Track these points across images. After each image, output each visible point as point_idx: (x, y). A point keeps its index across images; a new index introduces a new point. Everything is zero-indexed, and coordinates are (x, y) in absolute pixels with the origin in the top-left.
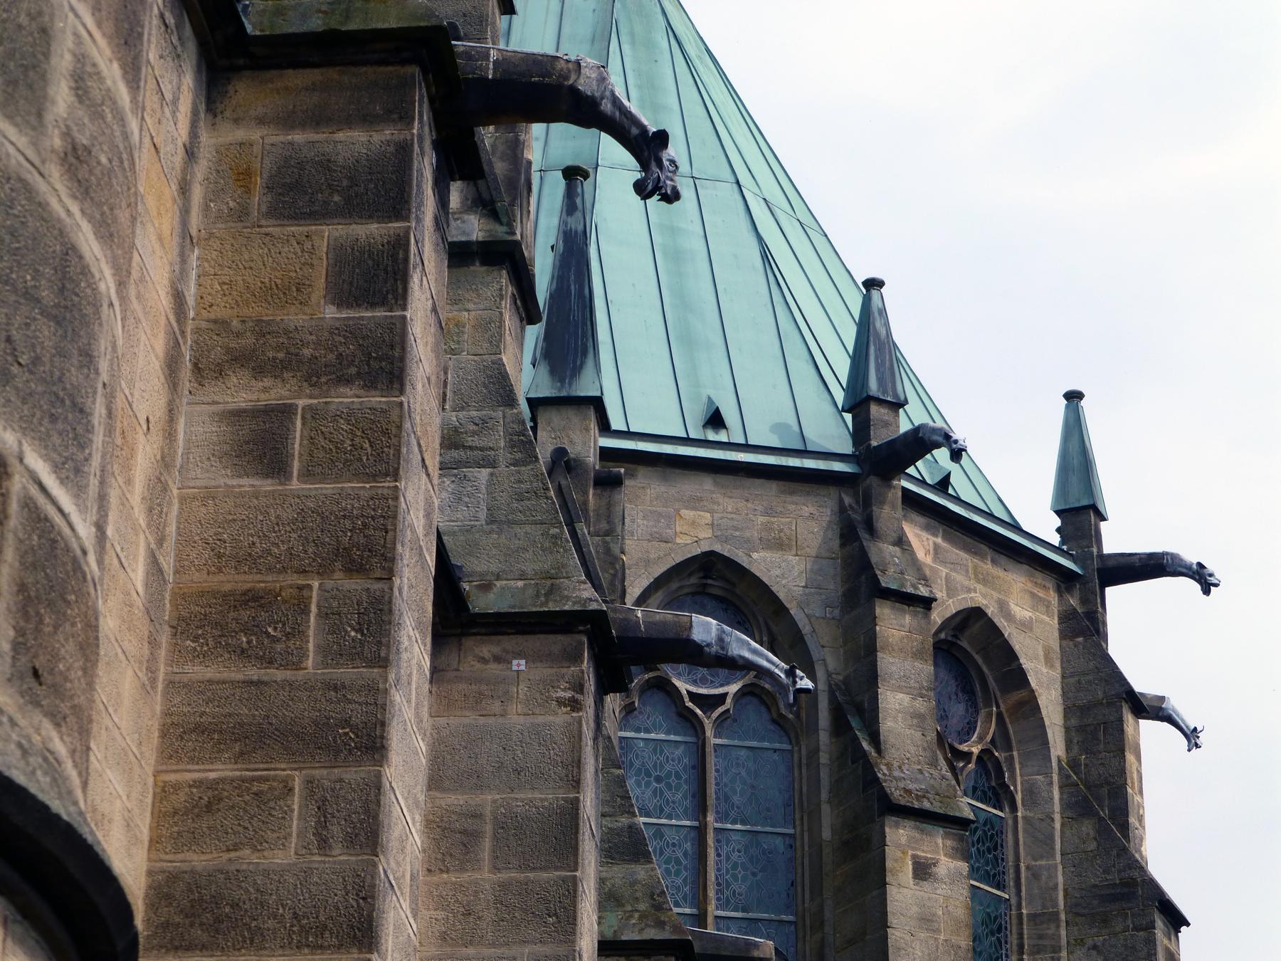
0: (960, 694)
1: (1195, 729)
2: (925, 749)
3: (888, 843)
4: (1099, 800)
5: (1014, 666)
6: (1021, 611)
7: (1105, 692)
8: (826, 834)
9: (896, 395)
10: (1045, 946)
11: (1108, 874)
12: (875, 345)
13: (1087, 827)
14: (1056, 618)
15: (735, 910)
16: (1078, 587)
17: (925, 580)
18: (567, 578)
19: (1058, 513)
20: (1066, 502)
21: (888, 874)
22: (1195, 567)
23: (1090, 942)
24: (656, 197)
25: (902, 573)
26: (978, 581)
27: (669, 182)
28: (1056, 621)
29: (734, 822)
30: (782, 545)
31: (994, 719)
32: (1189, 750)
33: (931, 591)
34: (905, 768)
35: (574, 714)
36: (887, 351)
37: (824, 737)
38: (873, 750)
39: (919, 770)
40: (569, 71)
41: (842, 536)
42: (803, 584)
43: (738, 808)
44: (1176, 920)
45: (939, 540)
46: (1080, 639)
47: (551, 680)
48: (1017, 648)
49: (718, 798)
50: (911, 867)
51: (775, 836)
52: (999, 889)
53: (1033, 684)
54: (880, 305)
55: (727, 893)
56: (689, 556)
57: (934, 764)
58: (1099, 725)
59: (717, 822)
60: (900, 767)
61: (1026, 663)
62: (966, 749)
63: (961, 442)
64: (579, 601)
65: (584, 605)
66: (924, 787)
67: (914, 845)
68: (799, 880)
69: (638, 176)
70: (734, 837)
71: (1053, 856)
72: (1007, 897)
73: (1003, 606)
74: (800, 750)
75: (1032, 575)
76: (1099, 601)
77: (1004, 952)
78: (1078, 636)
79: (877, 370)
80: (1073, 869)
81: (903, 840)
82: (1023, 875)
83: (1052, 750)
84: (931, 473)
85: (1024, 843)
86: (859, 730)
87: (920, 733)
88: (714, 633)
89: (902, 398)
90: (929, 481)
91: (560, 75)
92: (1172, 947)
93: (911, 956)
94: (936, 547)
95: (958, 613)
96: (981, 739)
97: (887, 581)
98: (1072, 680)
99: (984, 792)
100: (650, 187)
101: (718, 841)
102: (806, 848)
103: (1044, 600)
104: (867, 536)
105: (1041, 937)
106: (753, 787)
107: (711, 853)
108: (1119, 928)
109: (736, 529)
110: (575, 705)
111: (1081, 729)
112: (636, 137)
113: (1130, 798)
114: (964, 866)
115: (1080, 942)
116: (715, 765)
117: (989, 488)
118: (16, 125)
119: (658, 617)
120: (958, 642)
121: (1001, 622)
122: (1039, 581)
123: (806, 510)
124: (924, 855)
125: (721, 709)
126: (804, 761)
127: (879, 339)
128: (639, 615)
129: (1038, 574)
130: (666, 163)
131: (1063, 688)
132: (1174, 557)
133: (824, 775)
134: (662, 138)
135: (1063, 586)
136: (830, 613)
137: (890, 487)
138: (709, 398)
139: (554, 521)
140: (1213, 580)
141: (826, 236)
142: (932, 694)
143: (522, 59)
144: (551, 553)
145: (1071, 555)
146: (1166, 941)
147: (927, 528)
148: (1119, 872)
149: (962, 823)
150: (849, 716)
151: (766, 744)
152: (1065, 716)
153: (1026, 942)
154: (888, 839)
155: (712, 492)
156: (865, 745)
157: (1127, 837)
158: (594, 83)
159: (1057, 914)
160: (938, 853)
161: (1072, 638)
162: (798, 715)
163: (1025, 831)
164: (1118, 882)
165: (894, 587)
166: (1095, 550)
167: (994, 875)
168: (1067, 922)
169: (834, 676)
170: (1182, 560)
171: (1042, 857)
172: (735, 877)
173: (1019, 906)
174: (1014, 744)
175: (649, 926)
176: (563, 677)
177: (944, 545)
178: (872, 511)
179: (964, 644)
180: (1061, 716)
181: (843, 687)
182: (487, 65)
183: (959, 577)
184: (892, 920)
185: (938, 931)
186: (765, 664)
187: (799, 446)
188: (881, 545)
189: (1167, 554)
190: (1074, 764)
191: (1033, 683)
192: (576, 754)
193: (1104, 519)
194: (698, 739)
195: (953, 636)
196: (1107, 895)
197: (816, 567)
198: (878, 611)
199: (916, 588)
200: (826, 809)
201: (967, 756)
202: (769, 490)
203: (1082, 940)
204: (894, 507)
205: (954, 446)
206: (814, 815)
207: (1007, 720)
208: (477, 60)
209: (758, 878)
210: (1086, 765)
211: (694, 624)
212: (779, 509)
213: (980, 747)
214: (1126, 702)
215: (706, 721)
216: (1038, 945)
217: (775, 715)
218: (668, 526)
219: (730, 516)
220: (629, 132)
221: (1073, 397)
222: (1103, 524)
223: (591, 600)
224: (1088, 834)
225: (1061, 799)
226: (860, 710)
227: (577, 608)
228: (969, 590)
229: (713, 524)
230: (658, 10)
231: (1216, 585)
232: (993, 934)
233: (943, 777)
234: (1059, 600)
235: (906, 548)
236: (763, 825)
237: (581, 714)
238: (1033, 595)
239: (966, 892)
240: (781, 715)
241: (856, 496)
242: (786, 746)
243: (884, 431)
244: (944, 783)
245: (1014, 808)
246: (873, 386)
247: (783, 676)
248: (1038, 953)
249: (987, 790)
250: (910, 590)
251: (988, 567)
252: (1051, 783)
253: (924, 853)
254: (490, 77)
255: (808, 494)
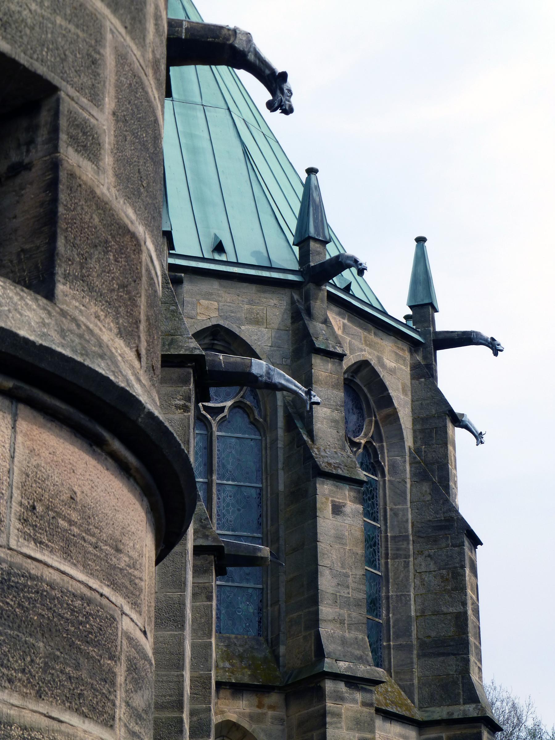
0: (355, 409)
1: (481, 433)
2: (338, 440)
3: (318, 493)
4: (432, 471)
5: (385, 394)
6: (390, 363)
7: (436, 410)
8: (281, 487)
9: (324, 236)
10: (401, 554)
11: (437, 514)
12: (313, 207)
13: (426, 487)
14: (409, 368)
15: (228, 530)
16: (421, 349)
17: (339, 343)
18: (181, 335)
19: (411, 307)
20: (415, 302)
21: (318, 511)
22: (489, 340)
23: (426, 553)
24: (279, 111)
25: (327, 340)
26: (367, 345)
27: (287, 102)
28: (409, 369)
29: (228, 480)
30: (258, 322)
31: (373, 424)
32: (477, 445)
33: (343, 350)
34: (327, 450)
35: (185, 414)
36: (320, 211)
37: (280, 432)
38: (309, 440)
39: (335, 452)
40: (230, 35)
41: (292, 318)
42: (270, 345)
43: (230, 472)
44: (476, 541)
45: (346, 321)
46: (423, 380)
47: (172, 394)
48: (387, 384)
49: (218, 466)
50: (330, 507)
51: (251, 488)
52: (374, 521)
53: (396, 405)
54: (316, 184)
55: (223, 520)
56: (205, 327)
57: (343, 449)
58: (433, 429)
59: (218, 479)
60: (324, 450)
61: (392, 393)
62: (358, 441)
63: (364, 265)
64: (188, 349)
65: (191, 351)
66: (338, 462)
67: (332, 495)
68: (264, 513)
69: (270, 97)
70: (228, 488)
71: (406, 503)
72: (379, 526)
73: (380, 359)
74: (266, 439)
75: (396, 343)
76: (433, 358)
77: (377, 557)
78: (421, 378)
79: (314, 221)
80: (417, 511)
81: (327, 492)
82: (388, 514)
83: (406, 443)
84: (340, 283)
85: (389, 495)
86: (301, 429)
87: (336, 431)
88: (264, 369)
89: (328, 238)
90: (338, 286)
91: (224, 38)
92: (473, 557)
93: (330, 558)
94: (344, 325)
95: (355, 363)
96: (366, 435)
97: (319, 344)
98: (417, 403)
99: (367, 466)
100: (276, 105)
101: (219, 490)
102: (269, 495)
103: (403, 357)
104: (307, 318)
105: (398, 549)
106: (239, 460)
107: (215, 497)
108: (444, 545)
109: (232, 312)
110: (186, 409)
111: (422, 431)
112: (268, 75)
113: (450, 471)
114: (360, 508)
115: (421, 553)
116: (218, 447)
117: (370, 291)
118: (136, 44)
119: (232, 360)
120: (354, 380)
121: (378, 369)
122: (400, 346)
123: (273, 302)
124: (337, 500)
125: (221, 415)
126: (268, 446)
127: (315, 203)
128: (221, 358)
129: (399, 342)
130: (286, 91)
131: (412, 407)
132: (477, 334)
133: (280, 454)
134: (284, 76)
135: (413, 349)
136: (285, 362)
137: (320, 290)
138: (215, 235)
139: (172, 302)
140: (500, 348)
141: (278, 142)
142: (343, 409)
143: (202, 27)
144: (171, 320)
145: (418, 331)
146: (470, 553)
147: (339, 314)
148: (444, 513)
149: (360, 483)
150: (296, 421)
151: (246, 436)
152: (413, 423)
153: (390, 552)
154: (318, 491)
155: (219, 290)
156: (305, 437)
157: (448, 493)
158: (245, 43)
159: (408, 536)
160: (346, 499)
161: (418, 379)
162: (265, 420)
163: (390, 488)
164: (443, 519)
165: (323, 347)
166: (432, 329)
167: (372, 513)
168: (413, 541)
169: (287, 397)
170: (482, 336)
171: (399, 504)
172: (228, 511)
173: (386, 531)
174: (384, 439)
175: (200, 537)
176: (179, 392)
177: (349, 324)
178: (310, 304)
179: (358, 381)
180: (411, 423)
181: (292, 404)
182: (182, 31)
183: (356, 343)
184: (320, 537)
185: (345, 544)
186: (294, 387)
187: (267, 265)
188: (315, 323)
189: (474, 332)
190: (418, 451)
191: (396, 404)
192: (187, 437)
193: (437, 311)
194: (208, 432)
195: (352, 376)
196: (437, 526)
197: (277, 335)
198: (313, 361)
199: (335, 348)
200: (281, 473)
201: (358, 445)
202: (251, 290)
203: (422, 552)
204: (322, 301)
205: (360, 267)
206: (274, 477)
207: (381, 425)
208: (175, 27)
209: (241, 512)
210: (425, 452)
211: (253, 364)
212: (257, 301)
213: (365, 440)
214: (449, 416)
215: (213, 422)
216: (397, 554)
217: (252, 420)
218: (193, 309)
219: (228, 304)
220: (264, 72)
221: (421, 240)
222: (436, 314)
223: (195, 348)
224: (426, 491)
225: (411, 471)
226: (301, 417)
227: (187, 353)
228: (362, 350)
229: (218, 309)
230: (181, 6)
231: (501, 351)
232: (371, 547)
233: (349, 457)
234: (411, 357)
235: (328, 325)
236: (244, 482)
237: (189, 414)
238: (397, 354)
239: (361, 523)
240: (255, 419)
241: (300, 295)
242: (258, 437)
243: (317, 257)
244: (349, 460)
245: (383, 475)
246: (312, 231)
247: (304, 395)
248: (397, 558)
249: (368, 464)
250: (331, 349)
251: (372, 337)
252: (405, 461)
253: (339, 500)
254: (183, 37)
255: (273, 292)
